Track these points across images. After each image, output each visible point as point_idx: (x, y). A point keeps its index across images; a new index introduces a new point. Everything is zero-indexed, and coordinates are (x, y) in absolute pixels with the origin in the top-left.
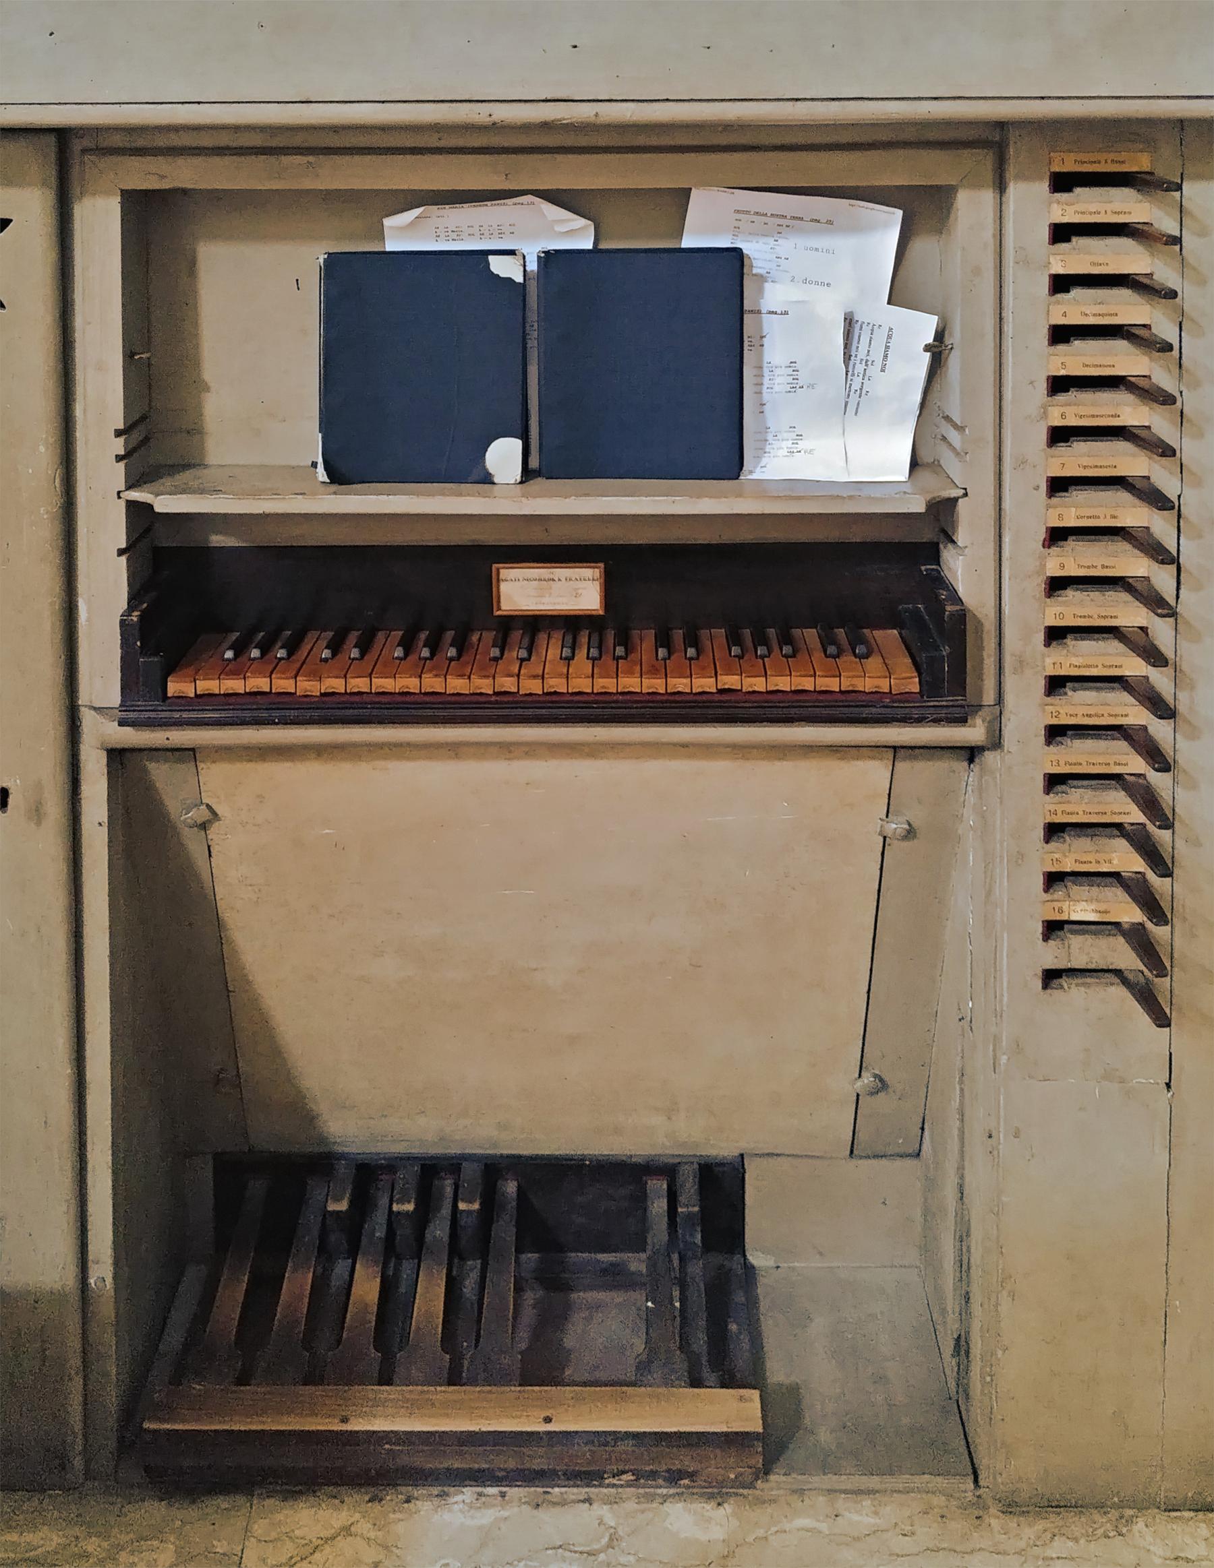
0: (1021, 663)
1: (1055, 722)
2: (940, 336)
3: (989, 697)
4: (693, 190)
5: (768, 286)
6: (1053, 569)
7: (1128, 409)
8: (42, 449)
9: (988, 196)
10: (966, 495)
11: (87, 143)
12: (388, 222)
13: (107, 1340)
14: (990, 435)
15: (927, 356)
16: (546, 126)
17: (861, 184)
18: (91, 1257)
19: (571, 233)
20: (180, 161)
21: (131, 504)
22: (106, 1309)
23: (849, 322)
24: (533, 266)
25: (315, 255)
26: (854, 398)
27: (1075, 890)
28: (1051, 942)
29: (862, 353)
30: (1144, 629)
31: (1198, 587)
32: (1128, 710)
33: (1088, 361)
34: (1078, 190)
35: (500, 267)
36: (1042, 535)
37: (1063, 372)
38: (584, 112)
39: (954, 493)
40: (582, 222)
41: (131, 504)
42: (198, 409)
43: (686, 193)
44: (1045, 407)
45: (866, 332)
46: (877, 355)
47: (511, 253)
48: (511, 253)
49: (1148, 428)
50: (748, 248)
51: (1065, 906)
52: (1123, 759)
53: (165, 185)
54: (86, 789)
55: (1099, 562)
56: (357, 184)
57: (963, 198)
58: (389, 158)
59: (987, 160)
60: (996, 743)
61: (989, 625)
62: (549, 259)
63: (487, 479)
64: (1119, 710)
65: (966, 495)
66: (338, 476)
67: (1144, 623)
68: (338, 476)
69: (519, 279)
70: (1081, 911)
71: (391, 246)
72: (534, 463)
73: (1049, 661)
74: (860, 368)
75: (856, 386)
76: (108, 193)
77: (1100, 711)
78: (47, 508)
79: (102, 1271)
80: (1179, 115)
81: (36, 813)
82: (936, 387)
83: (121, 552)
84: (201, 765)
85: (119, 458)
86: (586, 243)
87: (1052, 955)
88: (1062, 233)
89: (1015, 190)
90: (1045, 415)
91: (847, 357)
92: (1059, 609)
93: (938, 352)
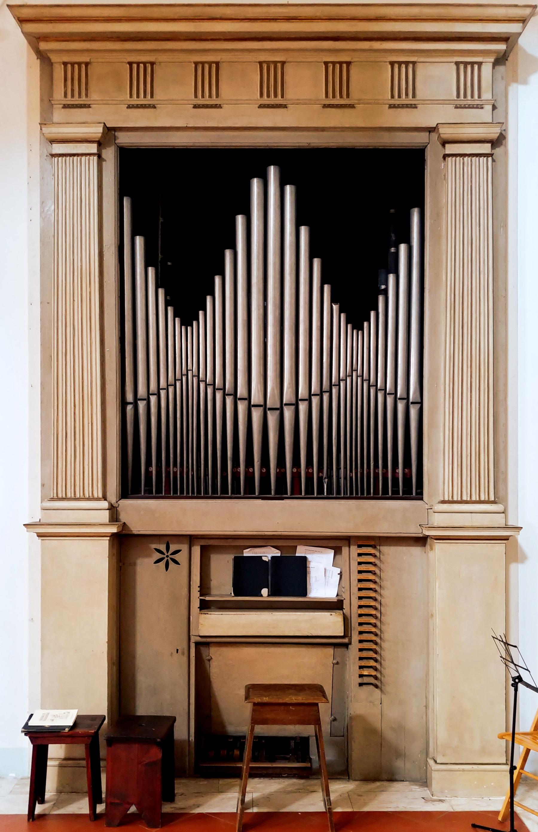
0: (354, 628)
1: (360, 639)
2: (341, 572)
3: (350, 635)
4: (298, 546)
5: (311, 563)
6: (359, 612)
7: (371, 585)
8: (186, 589)
9: (347, 548)
10: (345, 599)
11: (194, 537)
12: (244, 551)
13: (193, 751)
14: (349, 589)
15: (339, 576)
16: (273, 535)
17: (278, 545)
18: (190, 735)
19: (277, 553)
20: (211, 540)
21: (201, 600)
22: (193, 745)
23: (325, 569)
24: (270, 559)
25: (232, 557)
26: (327, 583)
27: (365, 669)
28: (360, 678)
29: (328, 575)
30: (375, 623)
31: (384, 616)
32: (373, 637)
33: (364, 576)
34: (363, 548)
35: (264, 559)
36: (357, 606)
37: (360, 578)
38: (280, 533)
39: (343, 599)
40: (278, 551)
41: (201, 600)
42: (210, 583)
43: (297, 546)
44: (357, 584)
45: (328, 571)
46: (330, 576)
47: (266, 556)
48: (266, 556)
49: (375, 588)
50: (307, 556)
51: (363, 672)
52: (372, 646)
53: (208, 544)
54: (191, 650)
55: (367, 611)
56: (238, 544)
57: (343, 548)
58: (251, 540)
59: (347, 542)
60: (350, 643)
61: (349, 618)
62: (273, 558)
63: (262, 596)
64: (372, 637)
65: (345, 599)
66: (236, 595)
67: (375, 622)
68: (236, 595)
69: (267, 561)
70: (366, 673)
71: (245, 555)
72: (270, 594)
73: (359, 628)
74: (327, 578)
75: (327, 581)
76: (198, 545)
77: (368, 637)
78: (186, 600)
79: (192, 738)
80: (379, 536)
81: (183, 654)
82: (341, 582)
83: (198, 608)
84: (210, 648)
85: (199, 591)
86: (279, 555)
87: (360, 680)
88: (360, 555)
89: (351, 547)
90: (357, 586)
91: (325, 576)
92: (361, 619)
93: (341, 574)
